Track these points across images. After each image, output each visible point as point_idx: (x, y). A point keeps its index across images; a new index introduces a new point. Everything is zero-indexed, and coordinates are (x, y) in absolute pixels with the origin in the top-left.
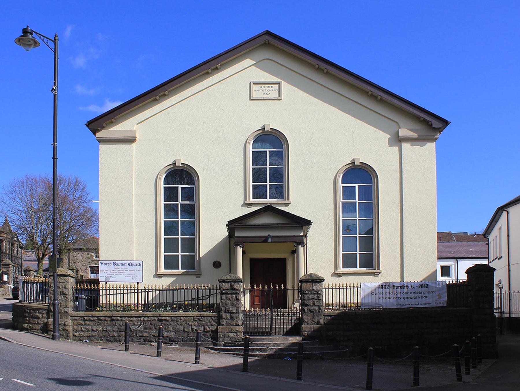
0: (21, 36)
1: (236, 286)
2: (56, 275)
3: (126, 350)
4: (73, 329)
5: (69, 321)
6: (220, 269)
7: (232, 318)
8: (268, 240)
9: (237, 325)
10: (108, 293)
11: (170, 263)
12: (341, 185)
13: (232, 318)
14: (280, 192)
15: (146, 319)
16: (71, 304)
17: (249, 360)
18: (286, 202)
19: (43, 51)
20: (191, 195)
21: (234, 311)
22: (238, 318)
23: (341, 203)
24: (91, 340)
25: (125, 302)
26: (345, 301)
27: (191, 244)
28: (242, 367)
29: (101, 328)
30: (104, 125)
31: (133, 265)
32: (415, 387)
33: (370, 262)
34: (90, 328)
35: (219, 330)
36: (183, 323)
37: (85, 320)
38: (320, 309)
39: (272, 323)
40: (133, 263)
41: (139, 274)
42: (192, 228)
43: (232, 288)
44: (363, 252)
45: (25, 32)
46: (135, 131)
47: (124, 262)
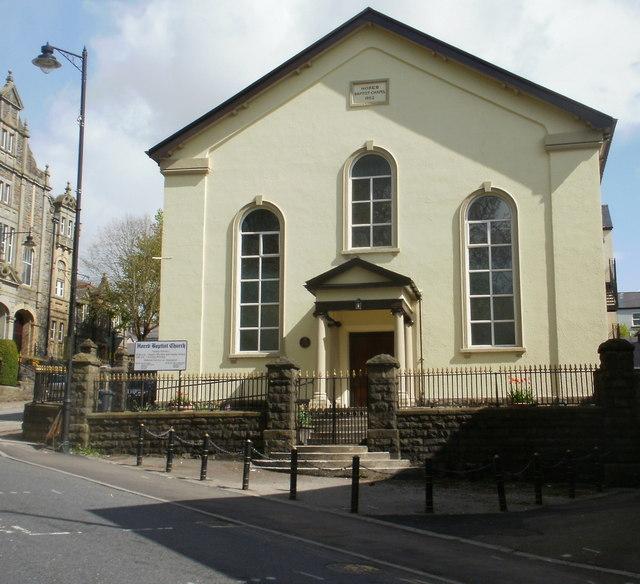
0: (40, 56)
1: (287, 373)
2: (71, 365)
3: (138, 464)
4: (90, 436)
5: (86, 426)
6: (304, 350)
7: (281, 419)
8: (365, 305)
9: (287, 428)
10: (182, 384)
11: (248, 342)
12: (467, 223)
13: (281, 419)
14: (385, 237)
15: (178, 421)
16: (90, 402)
17: (360, 481)
18: (393, 250)
19: (68, 71)
20: (274, 244)
21: (284, 408)
22: (288, 418)
23: (467, 251)
24: (108, 450)
25: (500, 396)
26: (446, 397)
27: (273, 316)
28: (350, 491)
29: (123, 435)
30: (170, 153)
31: (176, 346)
32: (429, 514)
33: (508, 335)
34: (109, 434)
35: (266, 436)
36: (222, 426)
37: (104, 426)
38: (391, 406)
39: (334, 424)
40: (176, 343)
41: (181, 359)
42: (274, 292)
43: (283, 377)
44: (495, 318)
45: (47, 50)
46: (207, 160)
47: (165, 343)
